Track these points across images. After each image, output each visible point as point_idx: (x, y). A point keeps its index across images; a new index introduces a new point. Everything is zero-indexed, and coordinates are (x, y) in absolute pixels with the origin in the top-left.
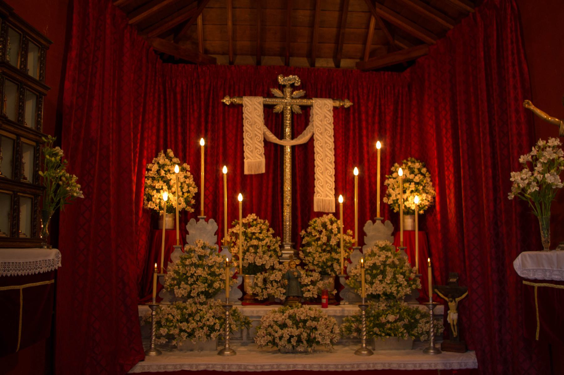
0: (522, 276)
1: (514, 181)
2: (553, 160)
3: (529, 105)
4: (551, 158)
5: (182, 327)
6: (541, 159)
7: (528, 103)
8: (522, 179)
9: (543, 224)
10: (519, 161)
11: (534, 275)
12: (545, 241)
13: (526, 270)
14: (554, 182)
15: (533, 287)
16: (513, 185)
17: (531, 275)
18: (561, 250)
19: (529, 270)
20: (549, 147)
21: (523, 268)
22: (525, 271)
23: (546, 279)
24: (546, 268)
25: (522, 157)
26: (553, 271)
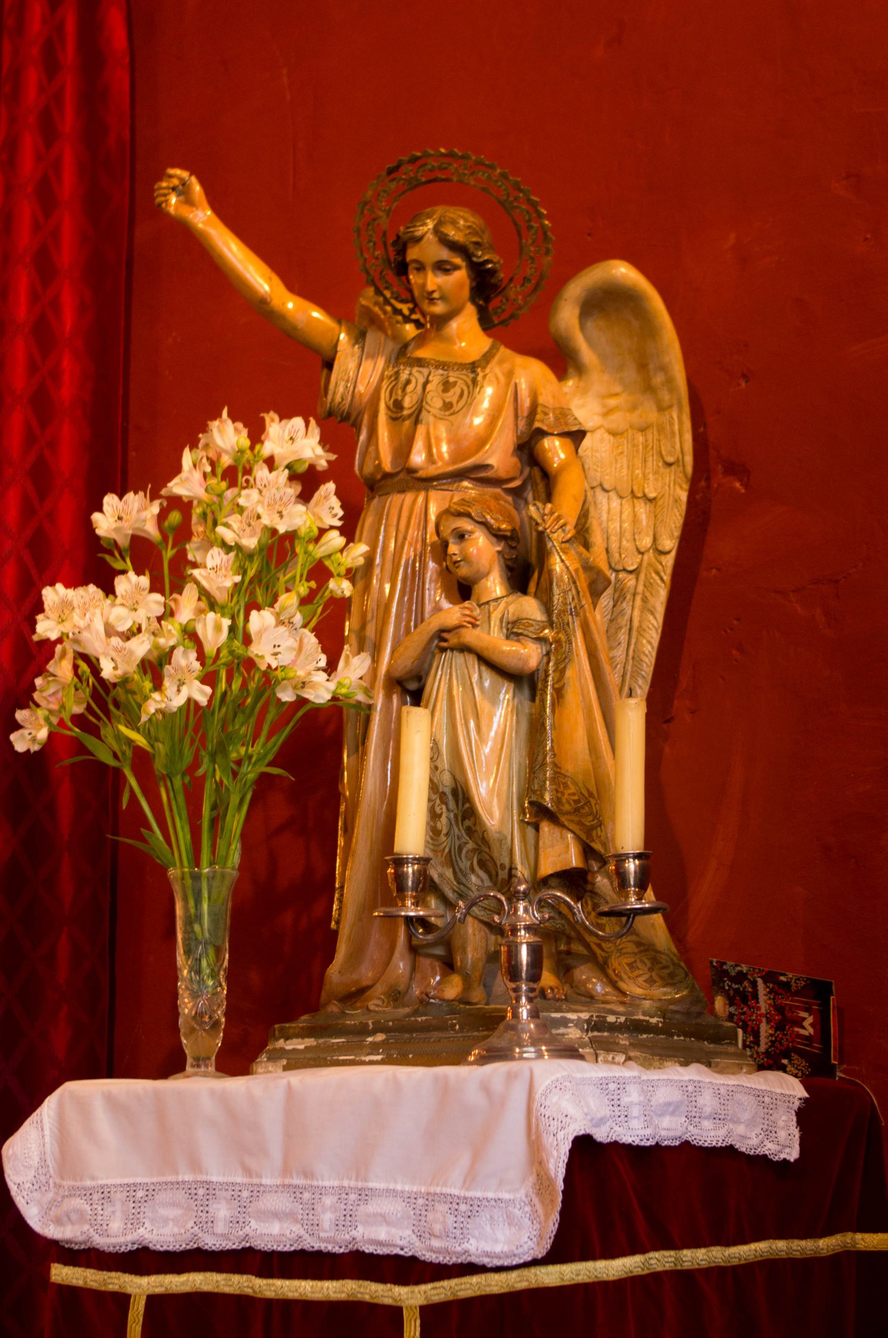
0: (51, 1232)
1: (60, 641)
2: (291, 536)
3: (187, 199)
4: (282, 529)
5: (287, 633)
6: (227, 525)
7: (183, 190)
8: (110, 631)
9: (199, 917)
10: (89, 528)
11: (134, 1221)
12: (198, 1016)
13: (87, 1193)
14: (294, 662)
15: (122, 1300)
16: (51, 667)
17: (116, 1225)
18: (286, 1068)
19: (106, 1194)
20: (270, 463)
21: (67, 1183)
22: (78, 1203)
23: (211, 1242)
24: (214, 1179)
25: (110, 501)
26: (257, 1191)
